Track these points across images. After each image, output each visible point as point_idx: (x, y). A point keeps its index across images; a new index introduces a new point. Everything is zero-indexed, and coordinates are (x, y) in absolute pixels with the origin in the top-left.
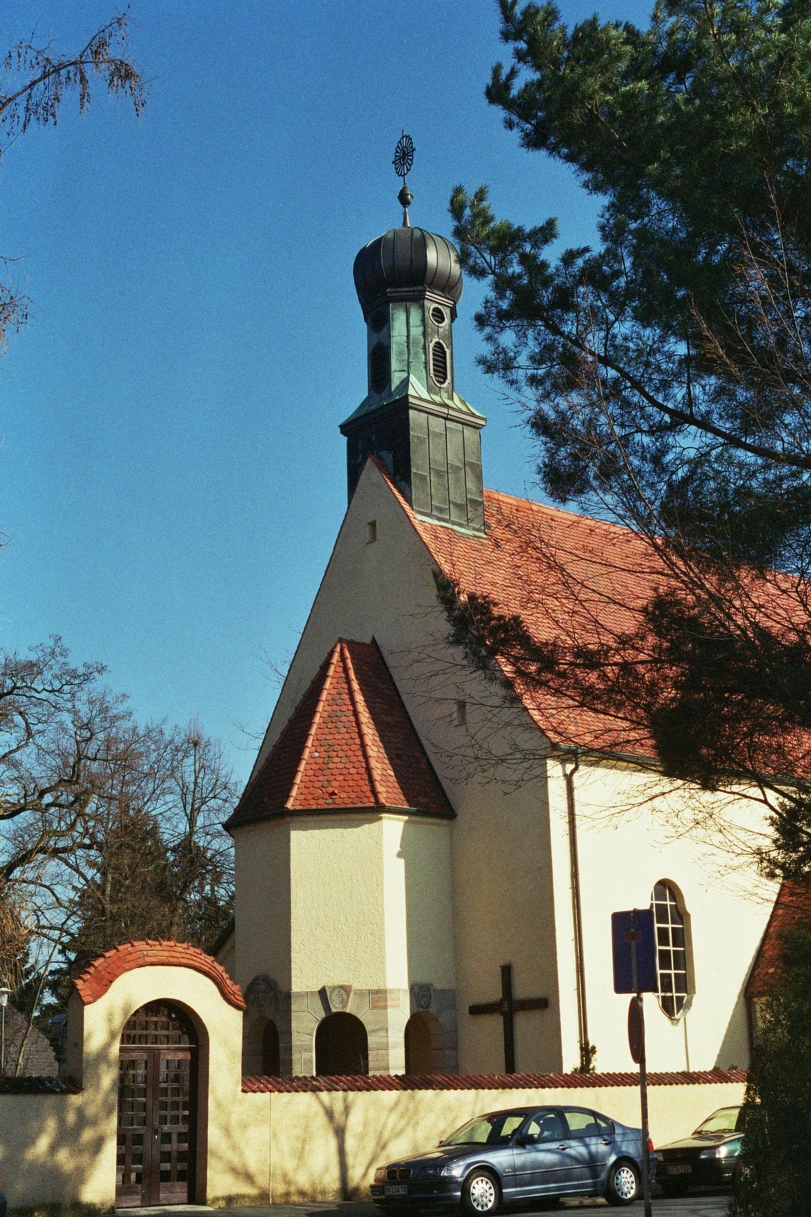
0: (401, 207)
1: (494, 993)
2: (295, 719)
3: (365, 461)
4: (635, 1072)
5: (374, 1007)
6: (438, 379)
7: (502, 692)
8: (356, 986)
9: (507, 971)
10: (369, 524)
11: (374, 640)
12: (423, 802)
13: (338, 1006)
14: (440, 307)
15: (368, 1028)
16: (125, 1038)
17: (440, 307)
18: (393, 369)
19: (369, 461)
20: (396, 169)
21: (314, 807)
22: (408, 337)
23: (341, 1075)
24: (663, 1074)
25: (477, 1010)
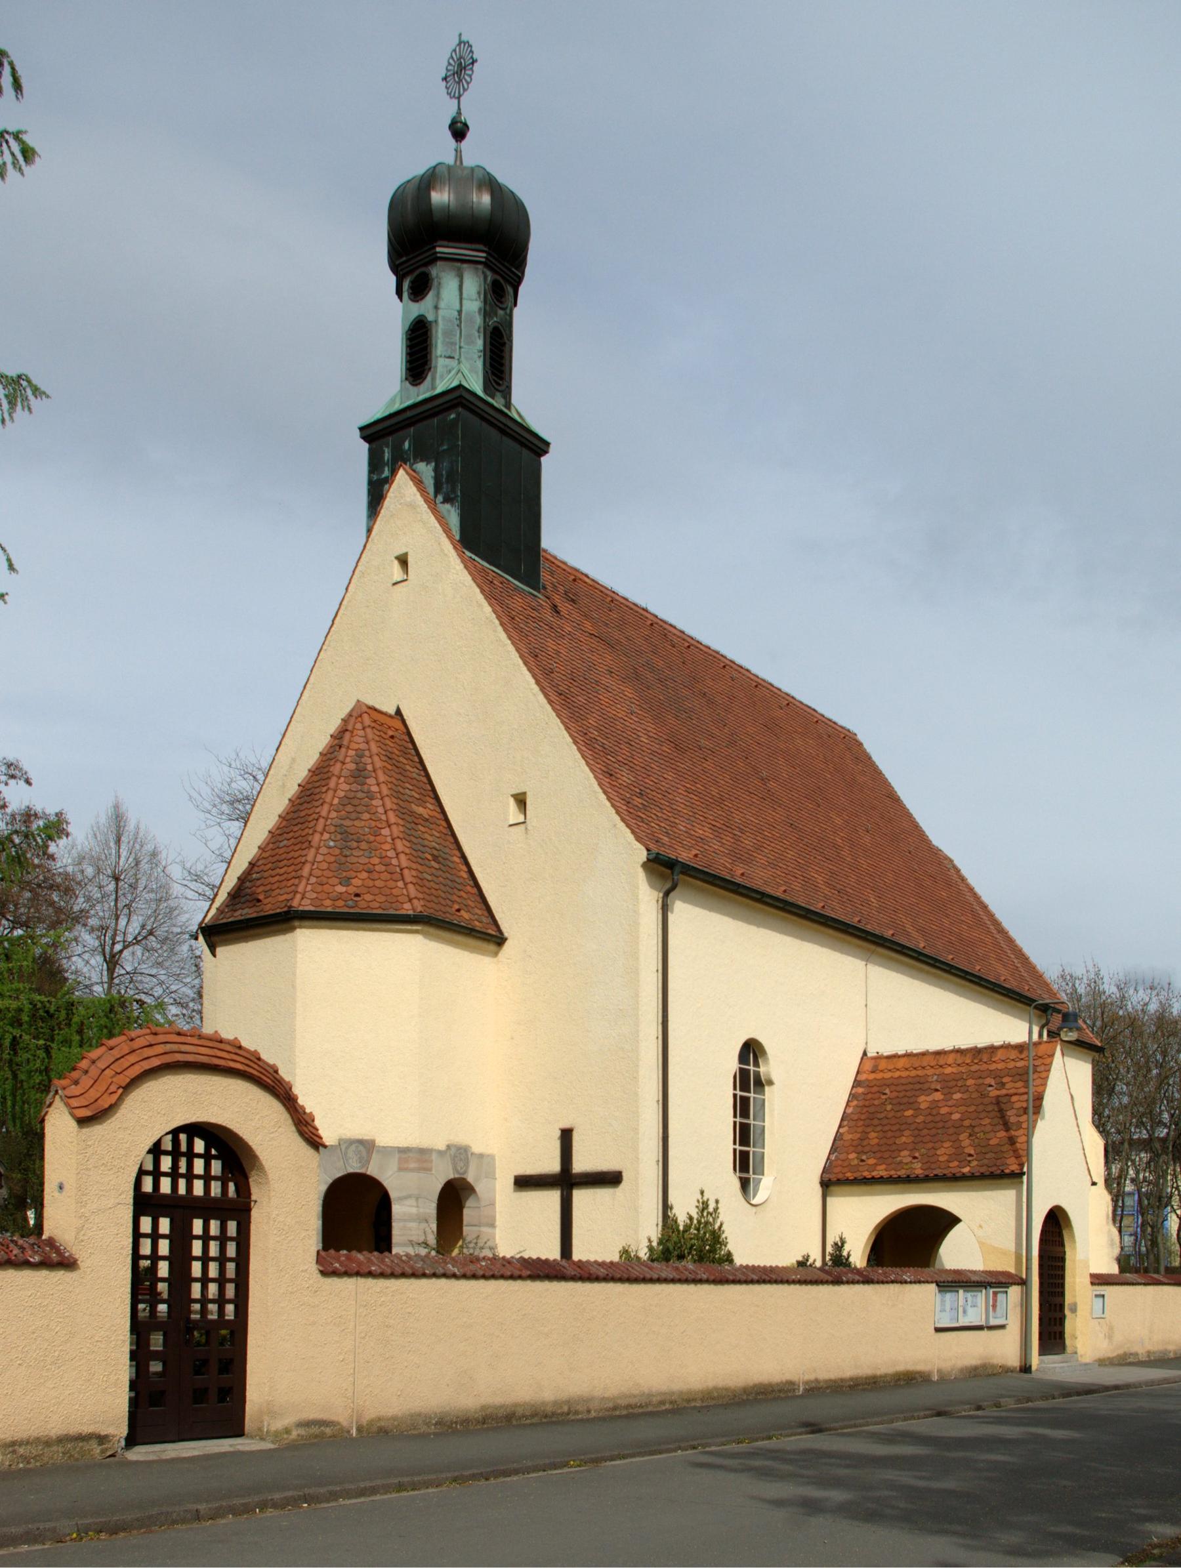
0: (453, 141)
1: (553, 1166)
2: (308, 783)
3: (394, 472)
4: (551, 1258)
5: (400, 1169)
6: (494, 377)
7: (108, 1010)
8: (383, 1140)
9: (566, 1136)
10: (397, 558)
11: (398, 712)
12: (467, 918)
13: (355, 1165)
14: (502, 281)
15: (393, 1195)
16: (1110, 1149)
17: (502, 281)
18: (439, 352)
19: (401, 472)
20: (472, 52)
21: (329, 909)
22: (460, 312)
23: (360, 1251)
24: (533, 1260)
25: (524, 1183)
